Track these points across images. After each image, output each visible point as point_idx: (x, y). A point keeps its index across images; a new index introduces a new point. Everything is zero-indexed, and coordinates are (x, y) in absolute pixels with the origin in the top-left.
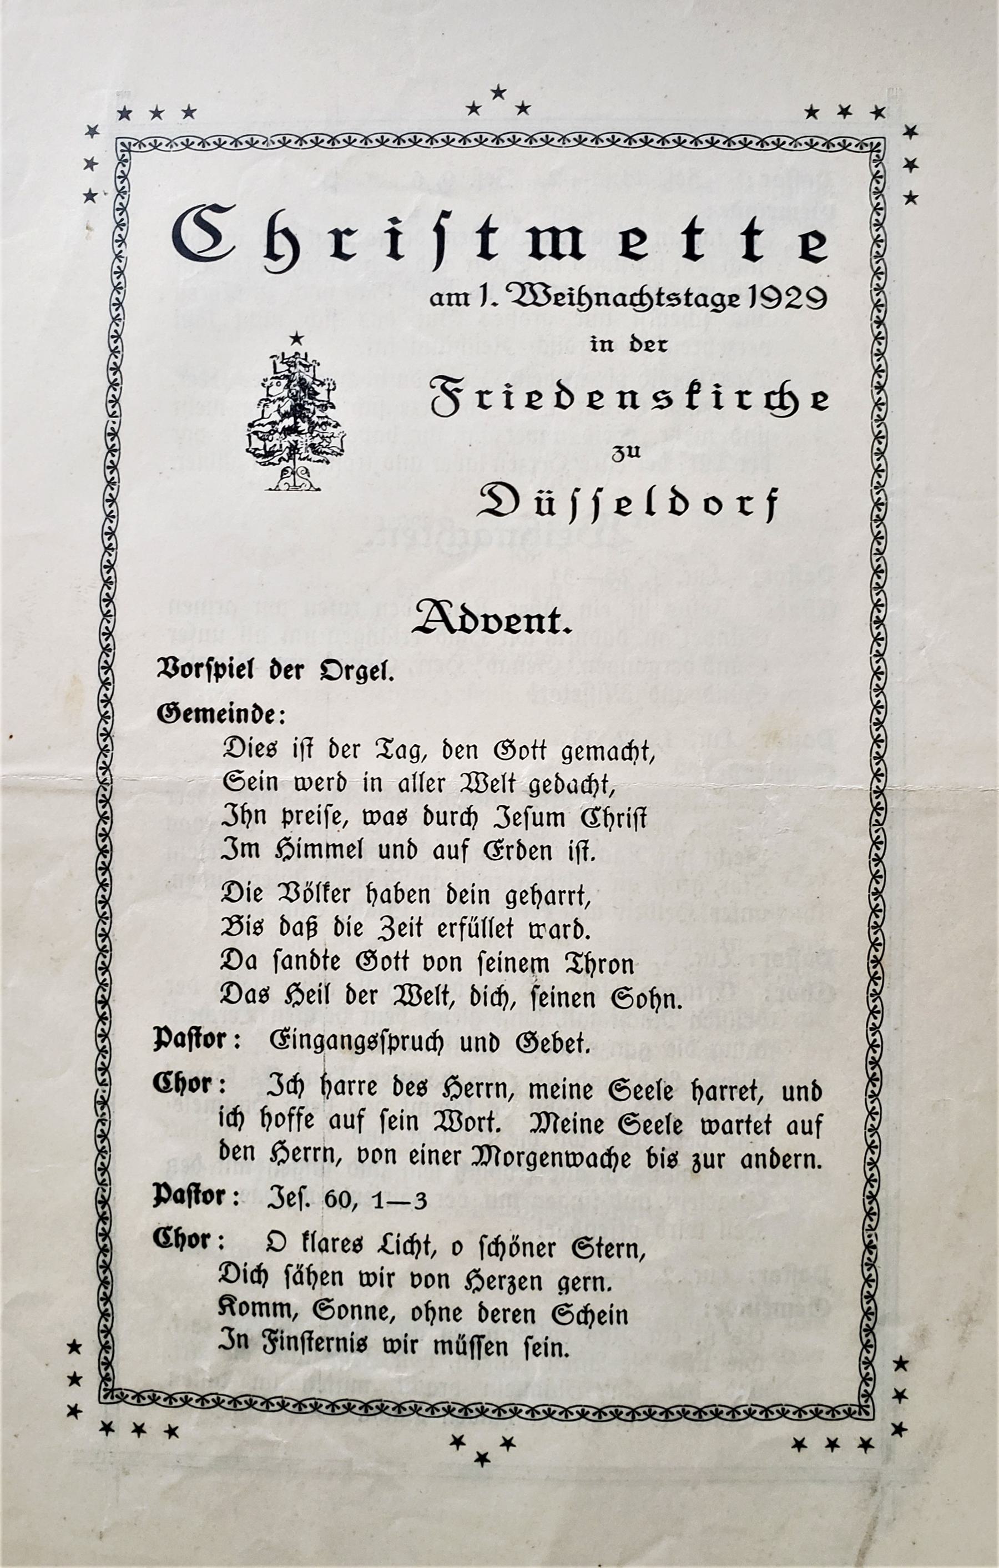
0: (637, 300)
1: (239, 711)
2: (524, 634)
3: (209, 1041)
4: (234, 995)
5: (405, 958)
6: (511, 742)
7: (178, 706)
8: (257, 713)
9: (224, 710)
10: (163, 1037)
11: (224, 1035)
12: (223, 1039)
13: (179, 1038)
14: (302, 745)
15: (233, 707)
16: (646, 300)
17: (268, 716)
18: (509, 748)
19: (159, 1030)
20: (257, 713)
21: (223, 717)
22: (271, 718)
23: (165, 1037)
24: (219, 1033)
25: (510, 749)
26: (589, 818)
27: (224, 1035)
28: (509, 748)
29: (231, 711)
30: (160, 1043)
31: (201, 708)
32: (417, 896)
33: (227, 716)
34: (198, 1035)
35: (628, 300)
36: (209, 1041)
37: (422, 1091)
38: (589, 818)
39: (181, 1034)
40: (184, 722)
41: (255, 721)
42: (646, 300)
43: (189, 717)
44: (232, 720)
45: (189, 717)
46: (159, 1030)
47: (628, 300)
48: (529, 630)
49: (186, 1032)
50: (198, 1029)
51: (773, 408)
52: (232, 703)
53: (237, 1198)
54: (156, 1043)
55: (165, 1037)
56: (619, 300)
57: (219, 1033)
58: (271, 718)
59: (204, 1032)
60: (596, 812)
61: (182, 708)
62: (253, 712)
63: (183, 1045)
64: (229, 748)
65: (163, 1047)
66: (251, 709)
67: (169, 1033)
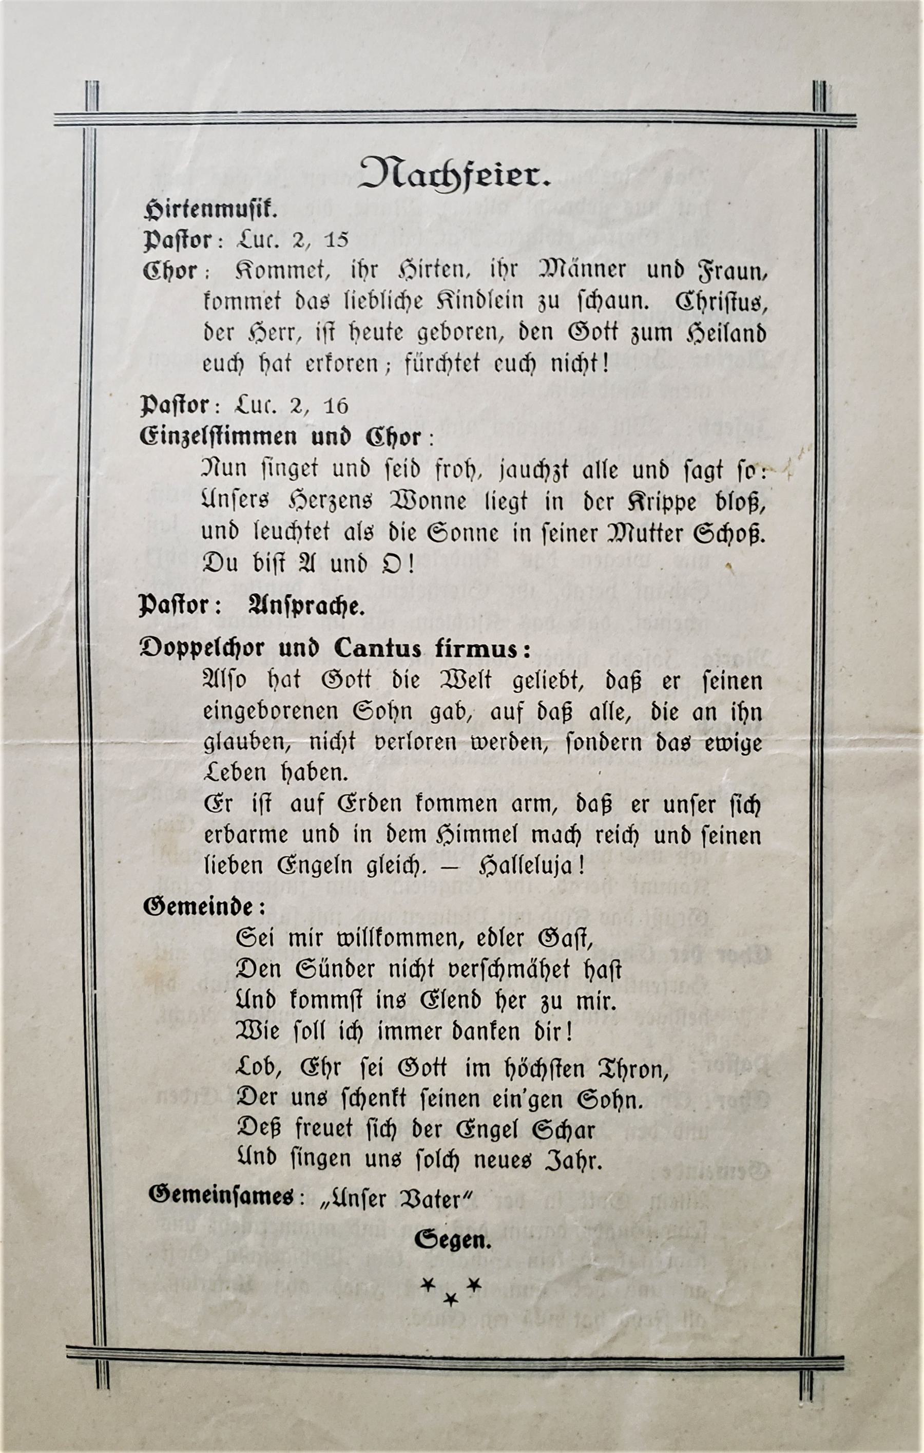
0: (439, 178)
1: (222, 1192)
2: (493, 187)
3: (193, 607)
4: (216, 564)
5: (443, 1064)
6: (554, 930)
7: (167, 1187)
8: (236, 905)
9: (208, 1191)
10: (148, 603)
11: (207, 601)
12: (205, 604)
13: (168, 240)
14: (275, 560)
15: (213, 900)
16: (451, 178)
17: (246, 908)
18: (553, 936)
19: (144, 597)
20: (236, 905)
21: (208, 1198)
22: (249, 910)
23: (150, 604)
24: (203, 400)
25: (553, 936)
26: (683, 301)
27: (207, 601)
28: (553, 936)
29: (211, 904)
30: (145, 610)
31: (188, 1189)
32: (445, 939)
33: (207, 909)
34: (185, 237)
35: (427, 179)
36: (193, 607)
37: (527, 1164)
38: (683, 301)
39: (170, 237)
40: (174, 1202)
41: (234, 913)
42: (451, 178)
43: (178, 1197)
44: (216, 1201)
45: (178, 1197)
46: (144, 597)
47: (427, 179)
48: (499, 183)
49: (174, 235)
50: (181, 596)
51: (437, 185)
52: (212, 897)
53: (221, 243)
54: (146, 245)
55: (151, 404)
56: (416, 178)
57: (203, 400)
58: (249, 910)
59: (187, 399)
60: (689, 296)
61: (171, 1189)
62: (233, 905)
63: (168, 411)
64: (208, 563)
65: (148, 613)
66: (230, 902)
67: (158, 236)
